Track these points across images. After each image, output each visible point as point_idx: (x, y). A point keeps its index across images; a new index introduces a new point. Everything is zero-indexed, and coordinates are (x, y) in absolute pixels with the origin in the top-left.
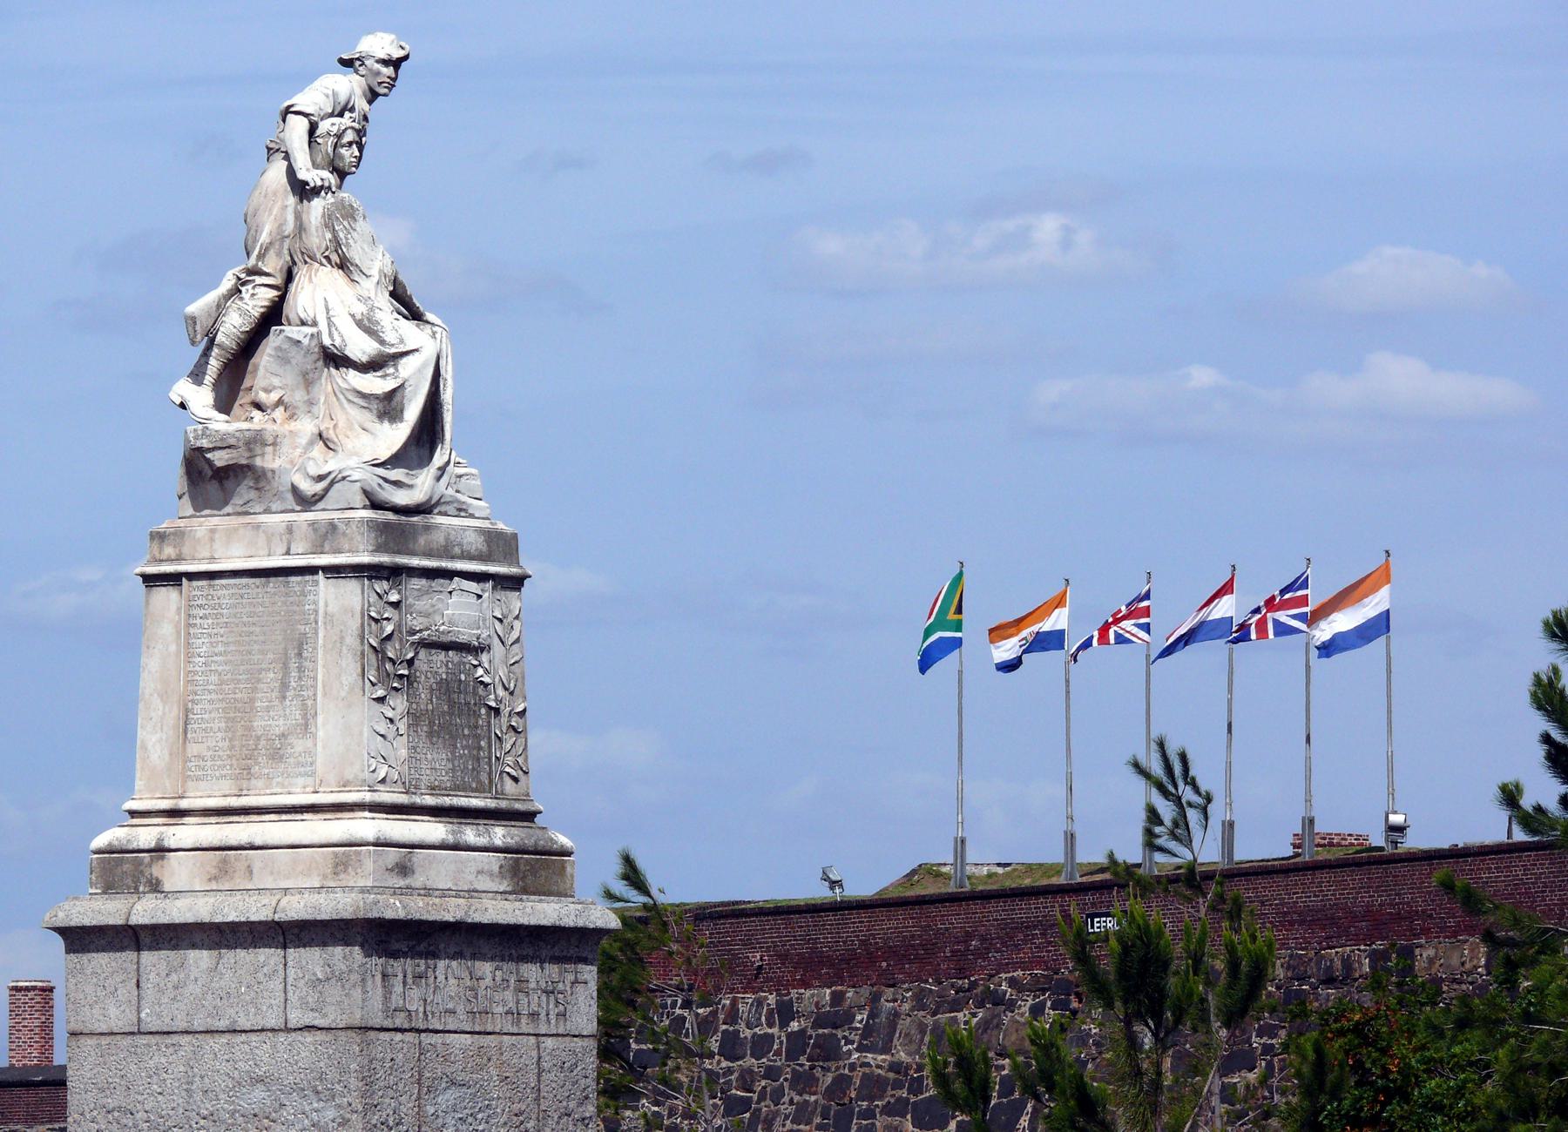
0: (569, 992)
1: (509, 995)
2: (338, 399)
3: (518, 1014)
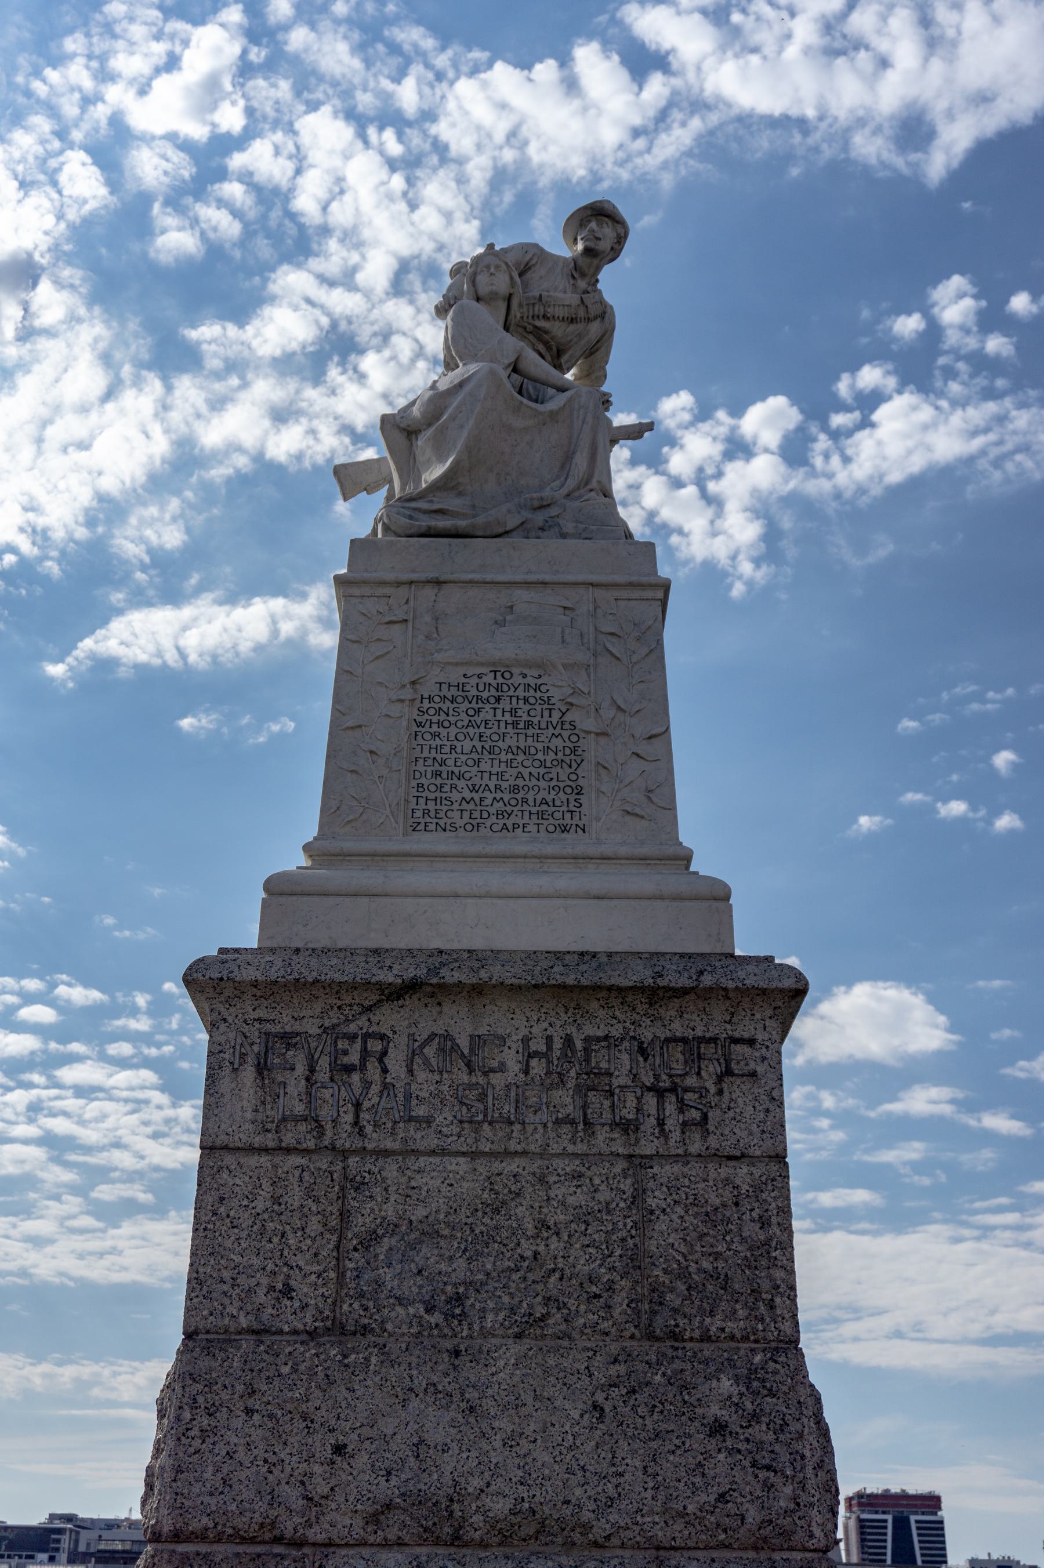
3: (586, 1123)
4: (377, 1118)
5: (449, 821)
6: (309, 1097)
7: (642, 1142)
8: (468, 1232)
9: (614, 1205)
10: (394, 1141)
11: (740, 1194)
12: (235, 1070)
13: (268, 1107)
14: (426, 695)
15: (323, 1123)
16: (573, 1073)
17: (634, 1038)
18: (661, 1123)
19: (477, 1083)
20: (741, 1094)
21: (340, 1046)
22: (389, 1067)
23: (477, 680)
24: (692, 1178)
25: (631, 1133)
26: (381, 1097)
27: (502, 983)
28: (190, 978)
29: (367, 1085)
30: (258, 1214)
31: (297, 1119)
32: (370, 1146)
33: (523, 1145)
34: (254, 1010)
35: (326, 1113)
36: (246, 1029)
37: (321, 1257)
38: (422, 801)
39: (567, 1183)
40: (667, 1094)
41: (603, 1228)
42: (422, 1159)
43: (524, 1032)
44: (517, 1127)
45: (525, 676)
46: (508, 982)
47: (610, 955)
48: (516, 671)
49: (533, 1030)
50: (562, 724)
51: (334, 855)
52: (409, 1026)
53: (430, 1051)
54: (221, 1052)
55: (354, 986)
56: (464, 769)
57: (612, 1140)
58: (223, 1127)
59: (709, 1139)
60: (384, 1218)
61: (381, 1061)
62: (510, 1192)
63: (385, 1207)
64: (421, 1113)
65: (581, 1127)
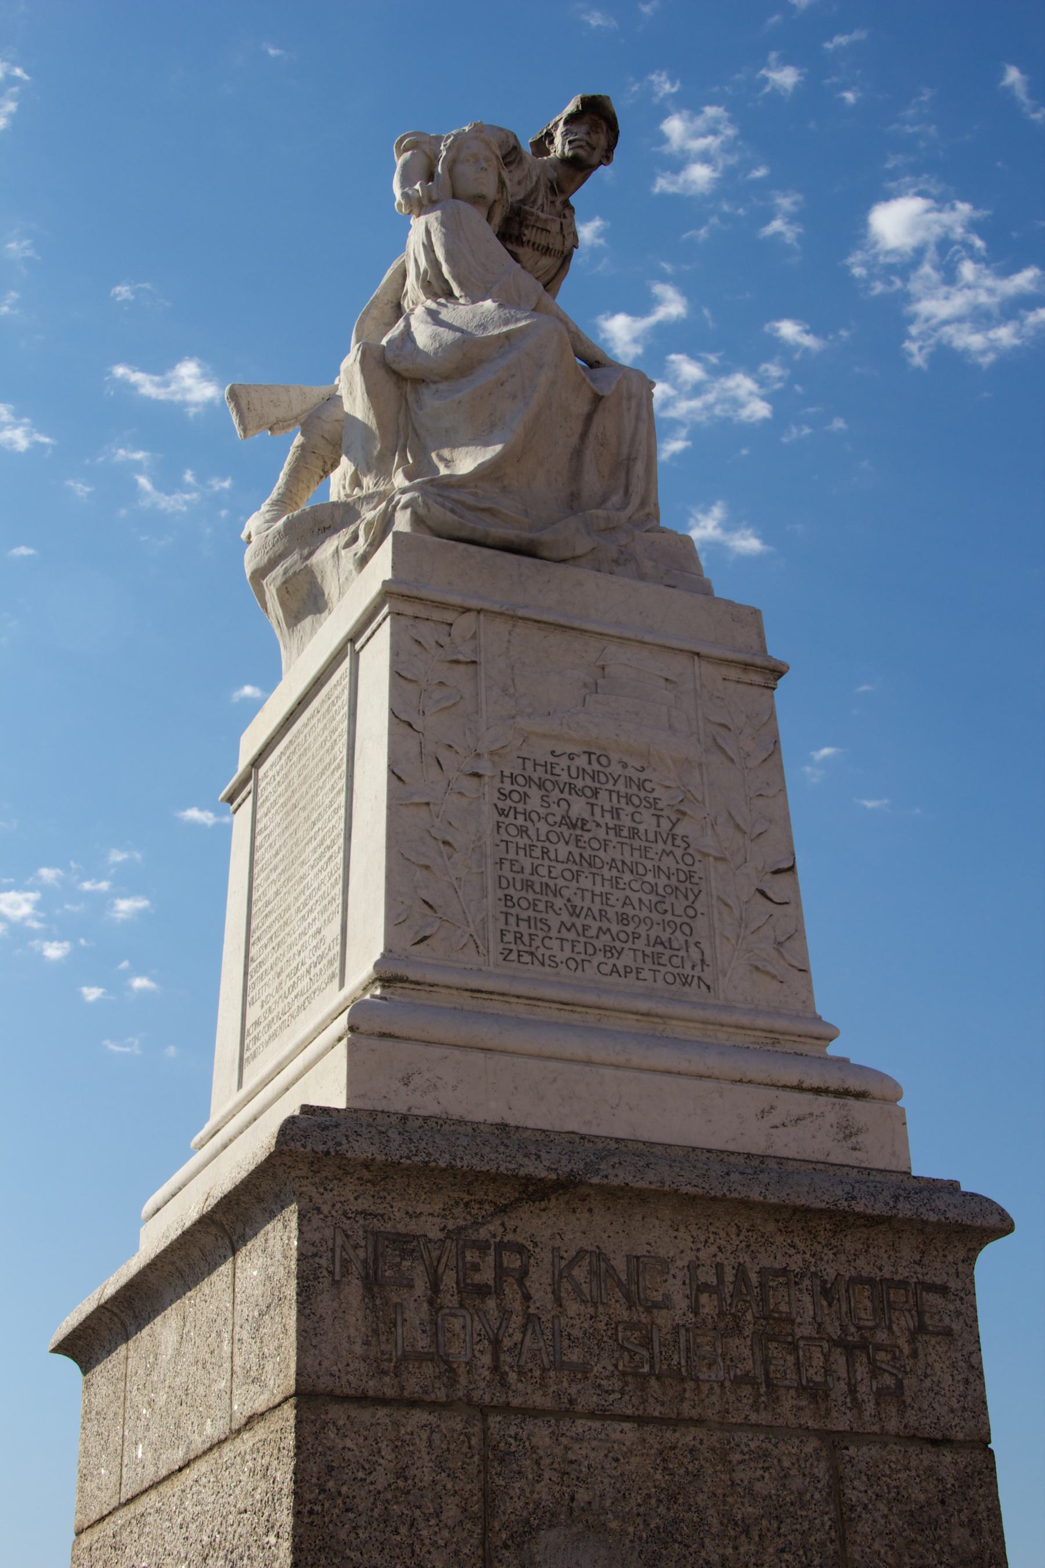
0: (906, 1351)
1: (740, 1347)
2: (804, 1043)
3: (769, 1383)
4: (522, 1363)
5: (548, 953)
6: (434, 1327)
7: (834, 1414)
8: (641, 1527)
9: (808, 1496)
10: (544, 1395)
11: (945, 1490)
12: (335, 1283)
13: (383, 1338)
14: (507, 773)
15: (455, 1366)
16: (749, 1317)
17: (815, 1274)
18: (852, 1390)
19: (640, 1321)
20: (937, 1358)
21: (468, 1258)
22: (532, 1292)
23: (569, 762)
24: (893, 1466)
25: (820, 1401)
26: (524, 1333)
27: (676, 1191)
28: (285, 1147)
29: (506, 1314)
30: (379, 1493)
31: (422, 1358)
32: (516, 1402)
33: (699, 1409)
34: (356, 1199)
35: (458, 1351)
36: (346, 1224)
37: (462, 1556)
38: (512, 920)
39: (752, 1464)
40: (857, 1352)
41: (798, 1526)
42: (579, 1422)
43: (689, 1256)
44: (690, 1385)
45: (625, 766)
46: (684, 1189)
47: (517, 1128)
48: (615, 757)
49: (701, 1254)
50: (674, 839)
51: (642, 1014)
52: (552, 1237)
53: (580, 1273)
54: (315, 1255)
55: (493, 1178)
56: (561, 882)
57: (800, 1409)
58: (326, 1363)
59: (907, 1415)
60: (537, 1504)
61: (521, 1282)
62: (687, 1472)
63: (538, 1487)
64: (574, 1358)
65: (763, 1390)
